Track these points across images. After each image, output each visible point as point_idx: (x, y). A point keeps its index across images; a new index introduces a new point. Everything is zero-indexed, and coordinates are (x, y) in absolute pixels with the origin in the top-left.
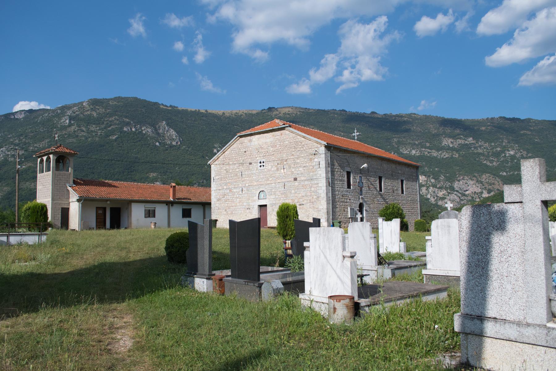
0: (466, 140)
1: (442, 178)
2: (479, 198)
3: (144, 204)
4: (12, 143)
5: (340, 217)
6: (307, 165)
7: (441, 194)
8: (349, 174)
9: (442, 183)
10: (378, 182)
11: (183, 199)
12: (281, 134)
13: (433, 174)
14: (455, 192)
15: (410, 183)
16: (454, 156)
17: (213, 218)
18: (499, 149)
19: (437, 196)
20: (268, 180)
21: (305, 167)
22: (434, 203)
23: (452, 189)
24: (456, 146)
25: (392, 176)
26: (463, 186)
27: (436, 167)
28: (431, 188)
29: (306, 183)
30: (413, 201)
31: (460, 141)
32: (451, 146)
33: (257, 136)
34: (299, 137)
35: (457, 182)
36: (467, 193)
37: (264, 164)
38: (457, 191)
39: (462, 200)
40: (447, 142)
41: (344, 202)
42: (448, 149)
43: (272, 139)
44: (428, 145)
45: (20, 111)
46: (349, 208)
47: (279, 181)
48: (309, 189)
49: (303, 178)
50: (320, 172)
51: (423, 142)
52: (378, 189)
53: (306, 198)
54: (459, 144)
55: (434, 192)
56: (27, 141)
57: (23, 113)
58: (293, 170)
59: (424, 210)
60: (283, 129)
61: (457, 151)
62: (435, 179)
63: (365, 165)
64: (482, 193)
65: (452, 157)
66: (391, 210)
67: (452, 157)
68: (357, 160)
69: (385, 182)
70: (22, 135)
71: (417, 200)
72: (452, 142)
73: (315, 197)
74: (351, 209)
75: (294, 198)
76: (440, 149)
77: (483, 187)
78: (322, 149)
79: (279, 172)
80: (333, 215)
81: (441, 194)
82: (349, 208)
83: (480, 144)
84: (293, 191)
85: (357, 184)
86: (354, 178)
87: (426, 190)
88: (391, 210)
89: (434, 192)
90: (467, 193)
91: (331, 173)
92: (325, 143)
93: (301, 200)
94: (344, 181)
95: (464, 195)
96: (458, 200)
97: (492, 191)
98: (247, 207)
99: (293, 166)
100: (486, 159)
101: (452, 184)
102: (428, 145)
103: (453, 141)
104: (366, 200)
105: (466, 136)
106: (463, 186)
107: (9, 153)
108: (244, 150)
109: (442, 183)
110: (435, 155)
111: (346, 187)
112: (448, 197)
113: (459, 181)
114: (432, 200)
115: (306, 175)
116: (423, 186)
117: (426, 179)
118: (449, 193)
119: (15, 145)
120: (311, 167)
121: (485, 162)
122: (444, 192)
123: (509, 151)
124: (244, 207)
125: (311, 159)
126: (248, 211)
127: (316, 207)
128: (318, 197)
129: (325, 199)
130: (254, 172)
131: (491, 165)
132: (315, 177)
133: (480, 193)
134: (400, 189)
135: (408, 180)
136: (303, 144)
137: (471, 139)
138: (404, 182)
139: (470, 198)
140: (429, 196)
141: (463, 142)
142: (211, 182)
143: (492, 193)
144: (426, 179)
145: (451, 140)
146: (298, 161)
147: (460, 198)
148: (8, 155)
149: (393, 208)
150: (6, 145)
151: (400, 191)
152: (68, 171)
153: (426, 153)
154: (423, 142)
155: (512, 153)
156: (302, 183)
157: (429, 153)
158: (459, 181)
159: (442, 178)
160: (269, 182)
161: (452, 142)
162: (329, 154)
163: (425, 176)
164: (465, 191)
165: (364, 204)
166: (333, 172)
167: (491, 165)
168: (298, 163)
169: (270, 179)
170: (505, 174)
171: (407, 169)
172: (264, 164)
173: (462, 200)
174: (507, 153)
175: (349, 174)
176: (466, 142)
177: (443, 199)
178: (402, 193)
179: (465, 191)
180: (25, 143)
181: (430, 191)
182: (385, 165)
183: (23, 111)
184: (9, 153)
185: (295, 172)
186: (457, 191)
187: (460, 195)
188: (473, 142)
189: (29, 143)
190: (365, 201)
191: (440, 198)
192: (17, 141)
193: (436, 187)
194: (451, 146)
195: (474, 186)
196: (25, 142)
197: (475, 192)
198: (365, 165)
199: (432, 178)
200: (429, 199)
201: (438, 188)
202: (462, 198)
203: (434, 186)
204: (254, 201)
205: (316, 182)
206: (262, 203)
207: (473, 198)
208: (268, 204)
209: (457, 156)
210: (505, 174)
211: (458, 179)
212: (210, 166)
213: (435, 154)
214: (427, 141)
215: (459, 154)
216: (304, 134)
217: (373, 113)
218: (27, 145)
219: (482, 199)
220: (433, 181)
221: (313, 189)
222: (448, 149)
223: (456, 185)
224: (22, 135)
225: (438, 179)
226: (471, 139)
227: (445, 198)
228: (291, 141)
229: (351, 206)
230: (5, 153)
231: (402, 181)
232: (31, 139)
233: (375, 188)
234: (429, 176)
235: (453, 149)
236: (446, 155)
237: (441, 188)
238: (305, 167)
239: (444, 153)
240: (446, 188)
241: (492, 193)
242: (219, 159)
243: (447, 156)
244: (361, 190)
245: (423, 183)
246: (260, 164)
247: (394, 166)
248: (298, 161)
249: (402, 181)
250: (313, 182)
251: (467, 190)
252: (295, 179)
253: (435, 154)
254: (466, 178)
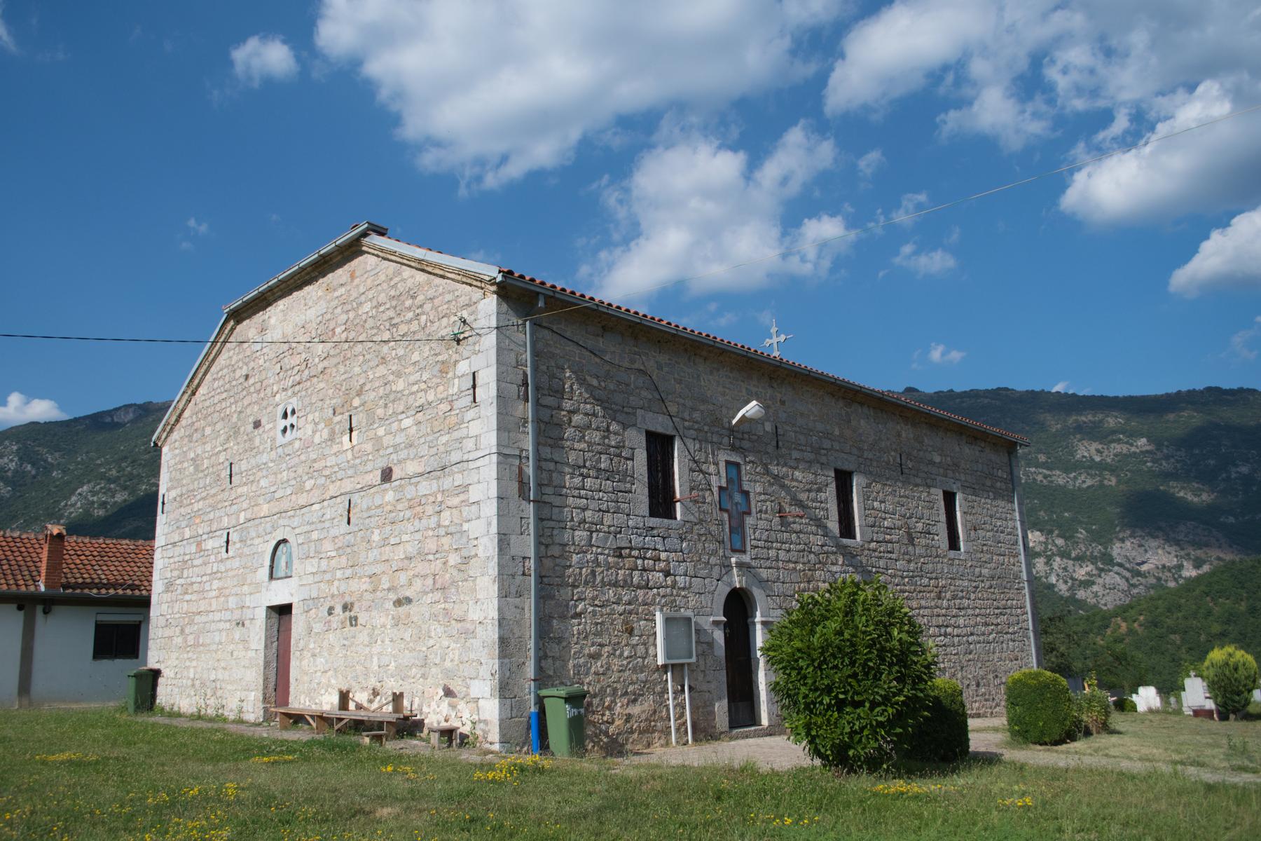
0: (1132, 445)
1: (1082, 534)
2: (1176, 580)
3: (93, 610)
4: (103, 477)
5: (598, 666)
6: (431, 397)
7: (1081, 572)
8: (660, 447)
9: (1081, 546)
10: (830, 493)
11: (107, 586)
12: (353, 277)
13: (1060, 527)
14: (1116, 568)
15: (987, 505)
16: (1106, 482)
17: (152, 663)
18: (1212, 462)
19: (1072, 578)
20: (300, 490)
21: (421, 409)
22: (1067, 594)
23: (1108, 560)
24: (1109, 460)
25: (904, 471)
26: (1134, 553)
27: (1066, 510)
28: (1058, 559)
29: (425, 487)
30: (1004, 580)
31: (1117, 448)
32: (1098, 459)
33: (282, 304)
34: (407, 272)
35: (1118, 545)
36: (1144, 568)
38: (1120, 565)
39: (1134, 586)
40: (1087, 450)
41: (627, 584)
42: (1090, 468)
43: (322, 307)
44: (1042, 458)
45: (125, 406)
46: (659, 618)
48: (433, 522)
49: (412, 468)
50: (475, 428)
51: (1030, 453)
52: (834, 525)
53: (421, 568)
54: (1116, 455)
55: (1065, 569)
56: (135, 472)
57: (131, 410)
58: (381, 432)
59: (1046, 613)
60: (352, 250)
61: (1113, 470)
62: (1066, 539)
63: (751, 408)
64: (1180, 567)
65: (1102, 485)
66: (833, 625)
67: (1102, 485)
68: (712, 383)
69: (865, 497)
70: (126, 458)
71: (1017, 577)
72: (1098, 451)
73: (454, 559)
74: (668, 621)
75: (377, 569)
76: (1071, 466)
77: (1183, 553)
78: (488, 307)
79: (336, 448)
80: (541, 658)
81: (1081, 572)
82: (659, 618)
83: (1165, 451)
84: (376, 537)
85: (713, 497)
86: (696, 466)
87: (1046, 563)
88: (833, 625)
89: (1065, 569)
90: (1144, 568)
91: (538, 434)
92: (492, 272)
93: (403, 578)
94: (627, 476)
95: (1139, 574)
96: (1123, 585)
97: (1204, 562)
98: (237, 615)
99: (380, 412)
100: (1183, 488)
101: (1106, 548)
102: (1042, 458)
103: (1100, 447)
104: (764, 574)
105: (1131, 436)
106: (1134, 553)
107: (95, 499)
108: (244, 372)
109: (1081, 546)
110: (1061, 481)
111: (643, 505)
112: (1100, 581)
113: (1123, 540)
114: (1063, 588)
115: (424, 450)
116: (1038, 555)
117: (1042, 539)
118: (1102, 570)
119: (110, 481)
120: (444, 407)
121: (1181, 494)
122: (1089, 569)
123: (1236, 466)
124: (228, 615)
125: (445, 369)
126: (238, 633)
127: (458, 611)
128: (466, 560)
129: (493, 569)
130: (265, 458)
131: (1196, 500)
132: (455, 457)
133: (1175, 567)
134: (942, 528)
135: (973, 489)
136: (421, 298)
137: (1144, 440)
138: (959, 498)
139: (1152, 581)
140: (1053, 579)
141: (1123, 448)
142: (155, 515)
143: (1206, 568)
144: (1042, 539)
145: (1095, 446)
146: (400, 385)
147: (1127, 580)
148: (93, 502)
149: (849, 612)
150: (89, 482)
151: (942, 539)
152: (854, 538)
153: (1040, 478)
154: (1030, 453)
155: (1245, 470)
156: (410, 492)
157: (1046, 477)
158: (1123, 540)
159: (1082, 534)
160: (302, 500)
161: (1098, 451)
162: (524, 336)
163: (1041, 531)
164: (1139, 564)
165: (758, 593)
166: (549, 431)
167: (1196, 500)
168: (397, 397)
170: (1231, 520)
171: (967, 450)
173: (1134, 586)
174: (1233, 469)
175: (660, 447)
176: (1133, 449)
177: (1087, 584)
178: (954, 544)
179: (1139, 564)
180: (131, 477)
181: (1055, 566)
182: (865, 425)
183: (130, 406)
184: (95, 499)
185: (388, 440)
186: (1120, 565)
187: (1128, 574)
188: (1148, 448)
189: (139, 475)
190: (762, 583)
191: (1081, 582)
192: (114, 472)
193: (1069, 558)
194: (1098, 459)
195: (1160, 551)
196: (131, 474)
197: (1164, 566)
198: (751, 408)
199: (1058, 536)
200: (1053, 586)
201: (1074, 559)
202: (1134, 581)
203: (1064, 555)
204: (257, 587)
205: (459, 479)
206: (279, 596)
207: (1159, 579)
208: (294, 600)
209: (1113, 481)
210: (1231, 520)
211: (1121, 535)
212: (157, 449)
213: (1060, 478)
214: (1040, 451)
215: (1118, 476)
216: (419, 253)
217: (910, 390)
218: (135, 481)
219: (1181, 581)
220: (1060, 542)
221: (446, 517)
222: (1090, 466)
223: (1117, 550)
224: (126, 458)
225: (1073, 537)
226: (1144, 440)
227: (1093, 583)
228: (382, 298)
229: (672, 604)
230: (85, 498)
231: (949, 498)
232: (144, 466)
233: (820, 524)
234: (1051, 532)
235: (1102, 467)
236: (1085, 481)
237: (1080, 559)
238: (421, 409)
239: (1083, 477)
240: (1093, 560)
241: (1206, 568)
242: (183, 422)
243: (1089, 482)
244: (738, 529)
245: (1037, 549)
246: (283, 423)
247: (907, 432)
248: (400, 385)
249: (949, 498)
250: (447, 483)
251: (1143, 563)
252: (387, 475)
253: (1060, 478)
254: (1140, 533)
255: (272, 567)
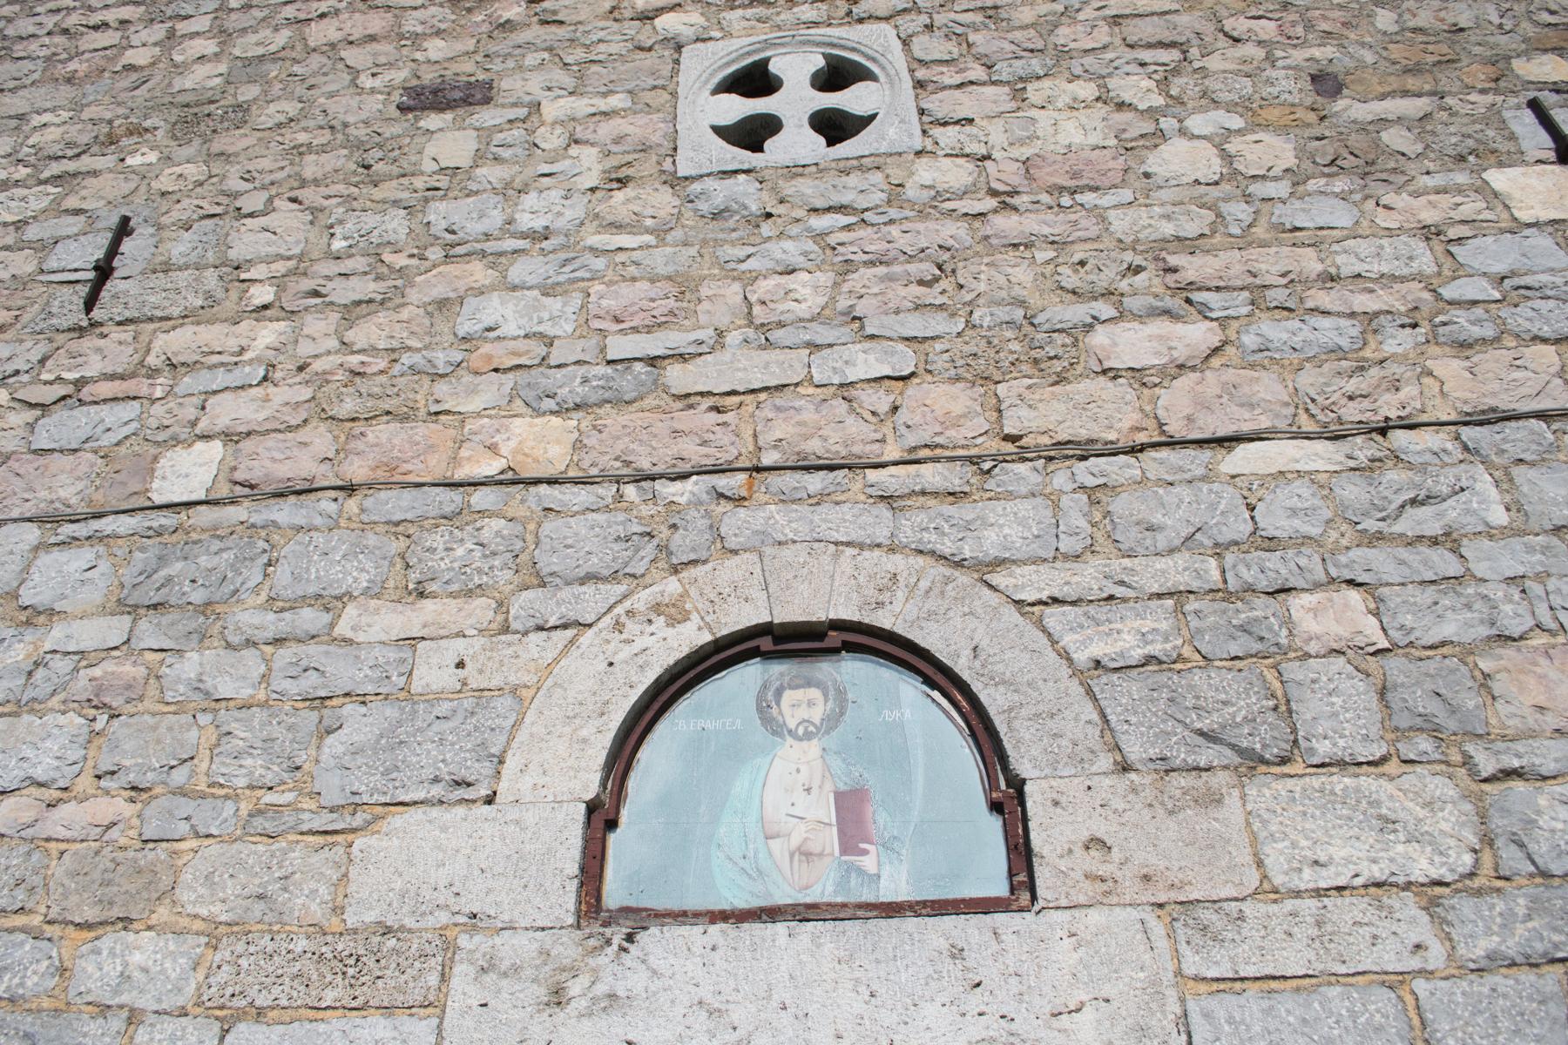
20: (1054, 358)
37: (796, 142)
47: (1458, 383)
169: (1133, 344)
172: (796, 142)
255: (602, 817)
